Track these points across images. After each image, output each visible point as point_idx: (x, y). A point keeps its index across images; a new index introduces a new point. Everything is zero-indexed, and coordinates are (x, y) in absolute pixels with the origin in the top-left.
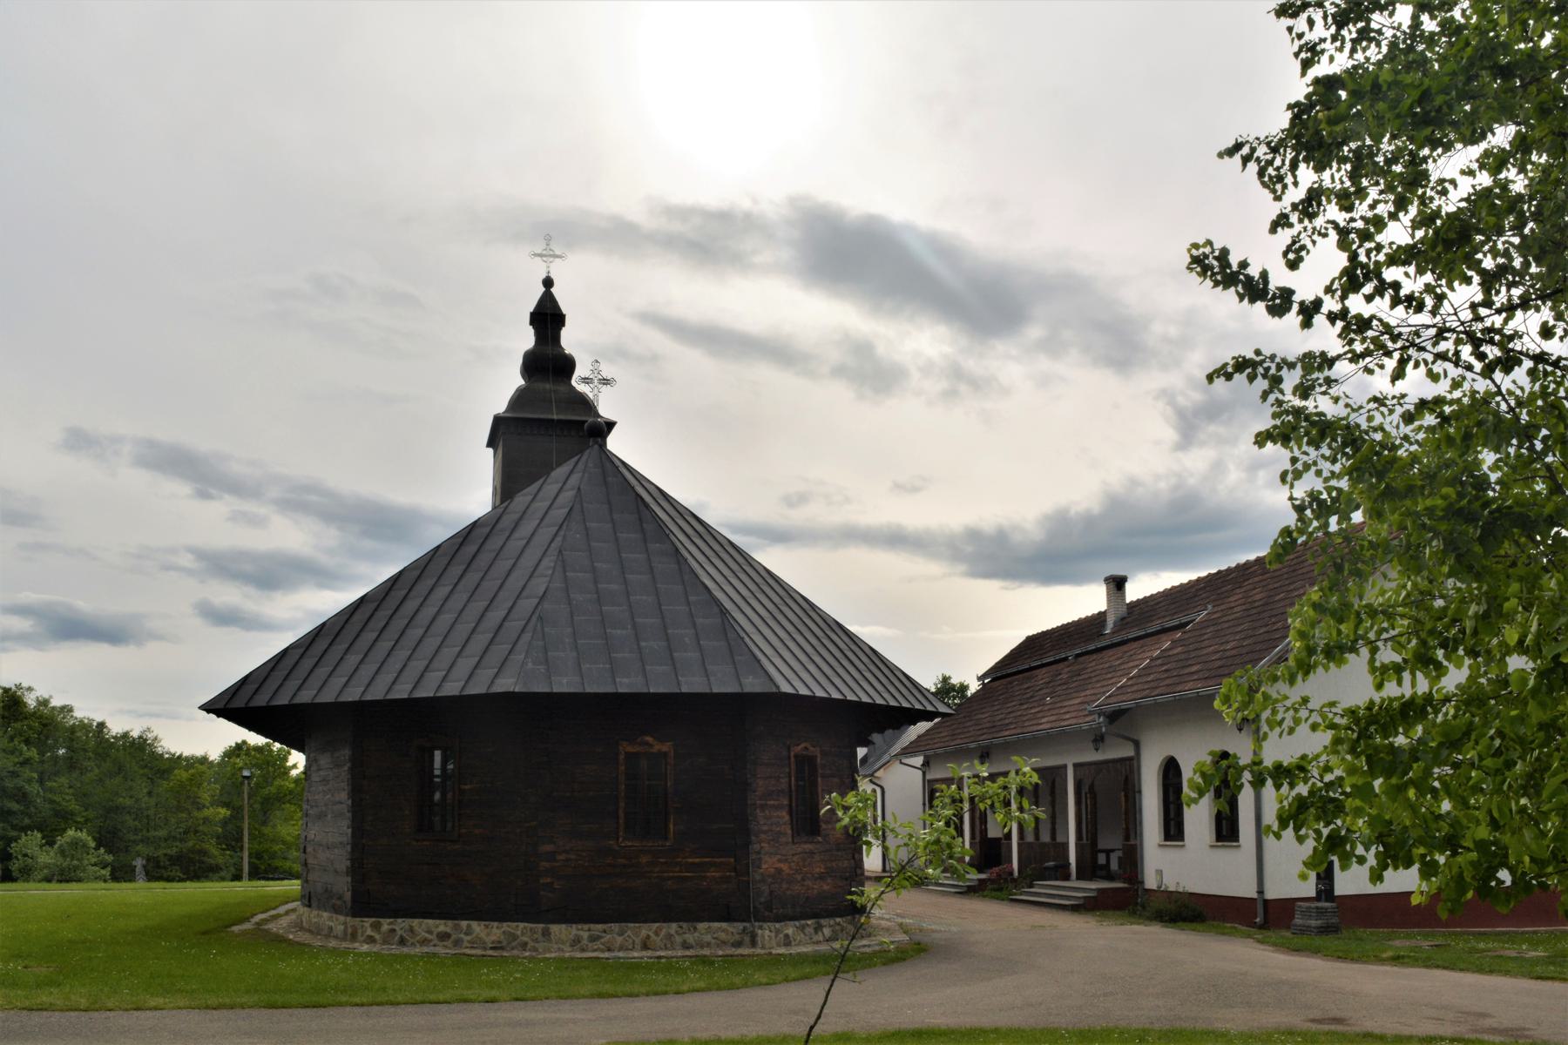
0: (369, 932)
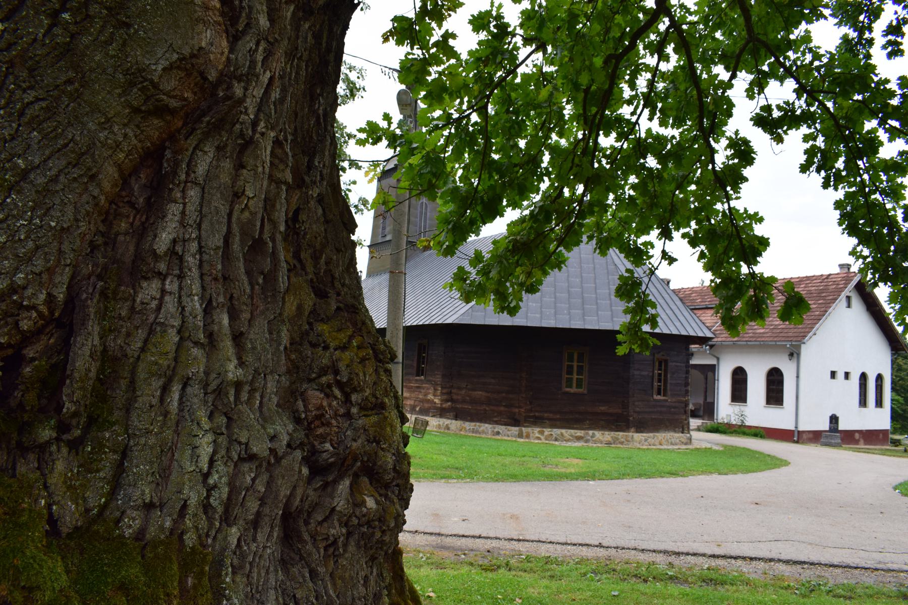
0: (537, 435)
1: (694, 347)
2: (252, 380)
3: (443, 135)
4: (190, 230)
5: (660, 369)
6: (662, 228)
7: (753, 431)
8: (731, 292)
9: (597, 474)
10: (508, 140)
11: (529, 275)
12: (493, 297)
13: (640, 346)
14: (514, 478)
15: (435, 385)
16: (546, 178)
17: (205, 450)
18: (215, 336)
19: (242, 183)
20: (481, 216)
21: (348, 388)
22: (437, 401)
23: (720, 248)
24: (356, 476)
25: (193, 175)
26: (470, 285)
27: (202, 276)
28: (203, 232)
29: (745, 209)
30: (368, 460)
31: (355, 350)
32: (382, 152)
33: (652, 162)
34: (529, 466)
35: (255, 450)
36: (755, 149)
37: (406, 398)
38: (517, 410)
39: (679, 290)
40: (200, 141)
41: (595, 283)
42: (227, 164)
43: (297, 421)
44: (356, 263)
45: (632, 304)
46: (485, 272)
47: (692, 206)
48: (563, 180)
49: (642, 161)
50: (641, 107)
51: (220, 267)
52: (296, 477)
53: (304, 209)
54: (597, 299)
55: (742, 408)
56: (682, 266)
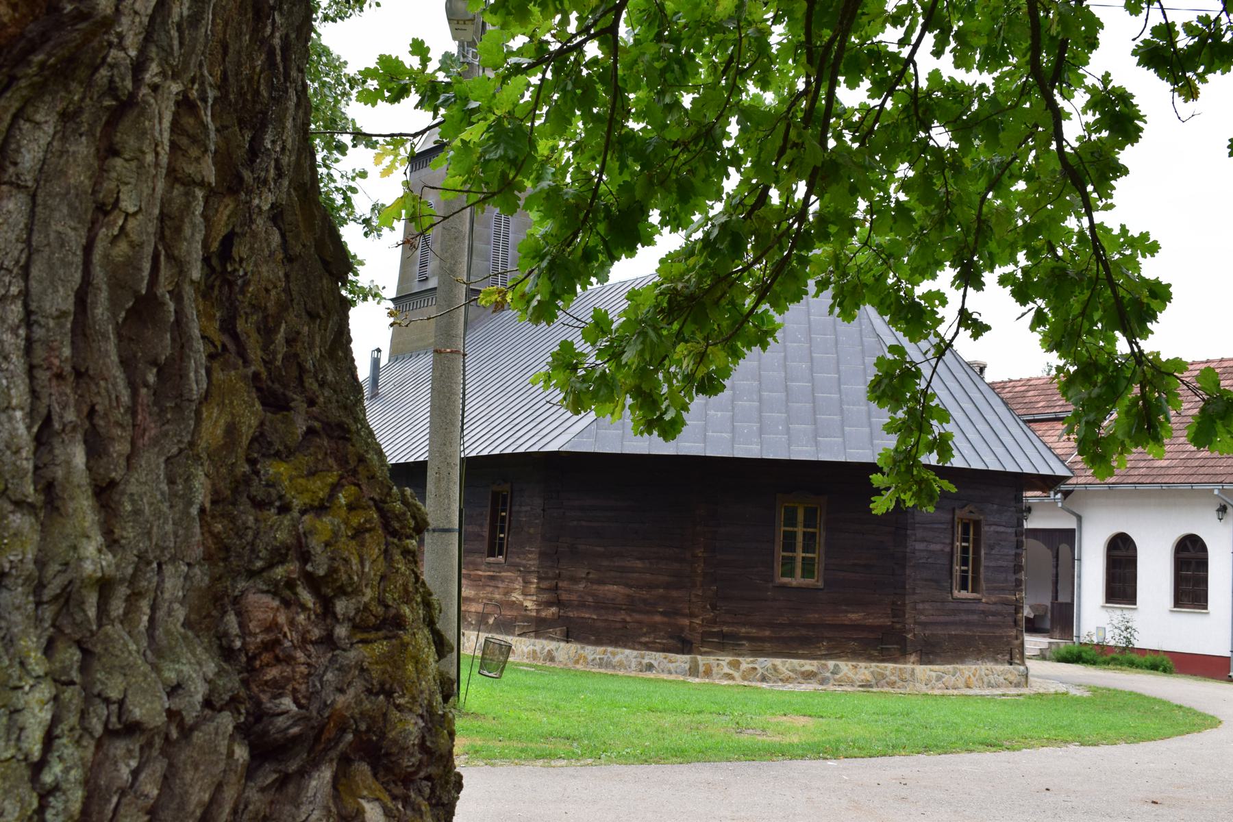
1: (1031, 496)
2: (134, 575)
3: (529, 85)
4: (7, 279)
5: (966, 540)
6: (963, 265)
7: (1149, 658)
8: (1096, 391)
9: (842, 746)
10: (661, 94)
11: (701, 358)
12: (629, 401)
13: (916, 495)
14: (680, 755)
15: (525, 573)
16: (732, 170)
17: (37, 717)
18: (58, 489)
19: (113, 185)
20: (605, 243)
21: (328, 590)
22: (529, 604)
23: (1076, 303)
24: (345, 761)
25: (11, 170)
26: (584, 379)
27: (31, 370)
28: (33, 284)
29: (1123, 227)
30: (369, 730)
31: (343, 512)
32: (409, 116)
33: (941, 137)
34: (710, 731)
35: (137, 713)
36: (1143, 109)
37: (468, 599)
38: (686, 622)
39: (1003, 385)
40: (27, 102)
41: (838, 372)
42: (82, 148)
43: (227, 653)
44: (350, 340)
45: (901, 414)
46: (613, 353)
47: (1020, 223)
48: (766, 175)
49: (922, 134)
50: (918, 29)
51: (67, 352)
52: (222, 766)
53: (244, 235)
54: (841, 401)
55: (1128, 614)
56: (1006, 340)
